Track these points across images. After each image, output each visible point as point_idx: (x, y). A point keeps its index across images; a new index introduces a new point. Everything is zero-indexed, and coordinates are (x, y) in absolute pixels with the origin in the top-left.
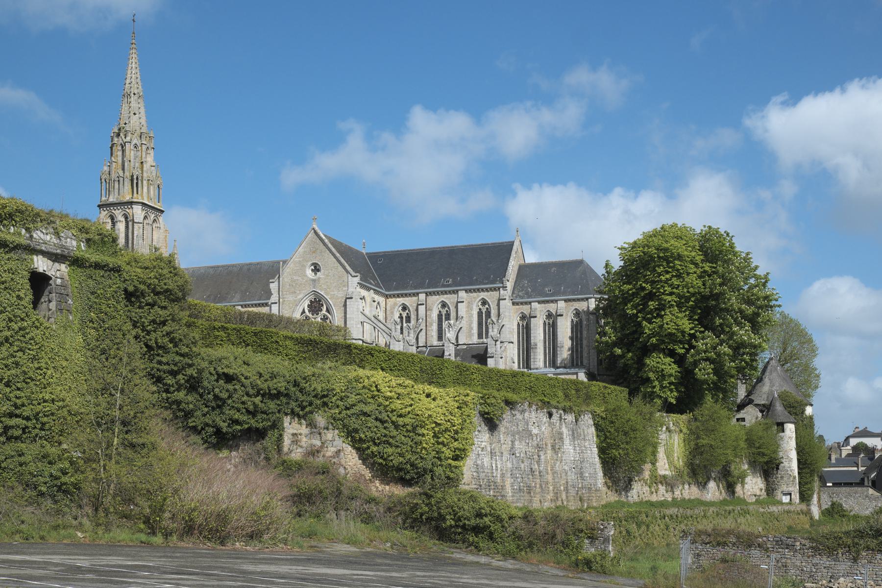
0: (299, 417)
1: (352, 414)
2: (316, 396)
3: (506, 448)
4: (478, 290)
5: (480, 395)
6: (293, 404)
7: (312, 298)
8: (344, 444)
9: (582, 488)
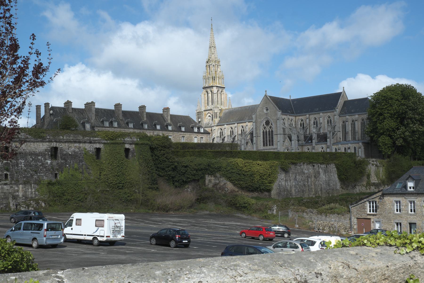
0: (211, 175)
2: (216, 169)
5: (280, 162)
9: (329, 189)
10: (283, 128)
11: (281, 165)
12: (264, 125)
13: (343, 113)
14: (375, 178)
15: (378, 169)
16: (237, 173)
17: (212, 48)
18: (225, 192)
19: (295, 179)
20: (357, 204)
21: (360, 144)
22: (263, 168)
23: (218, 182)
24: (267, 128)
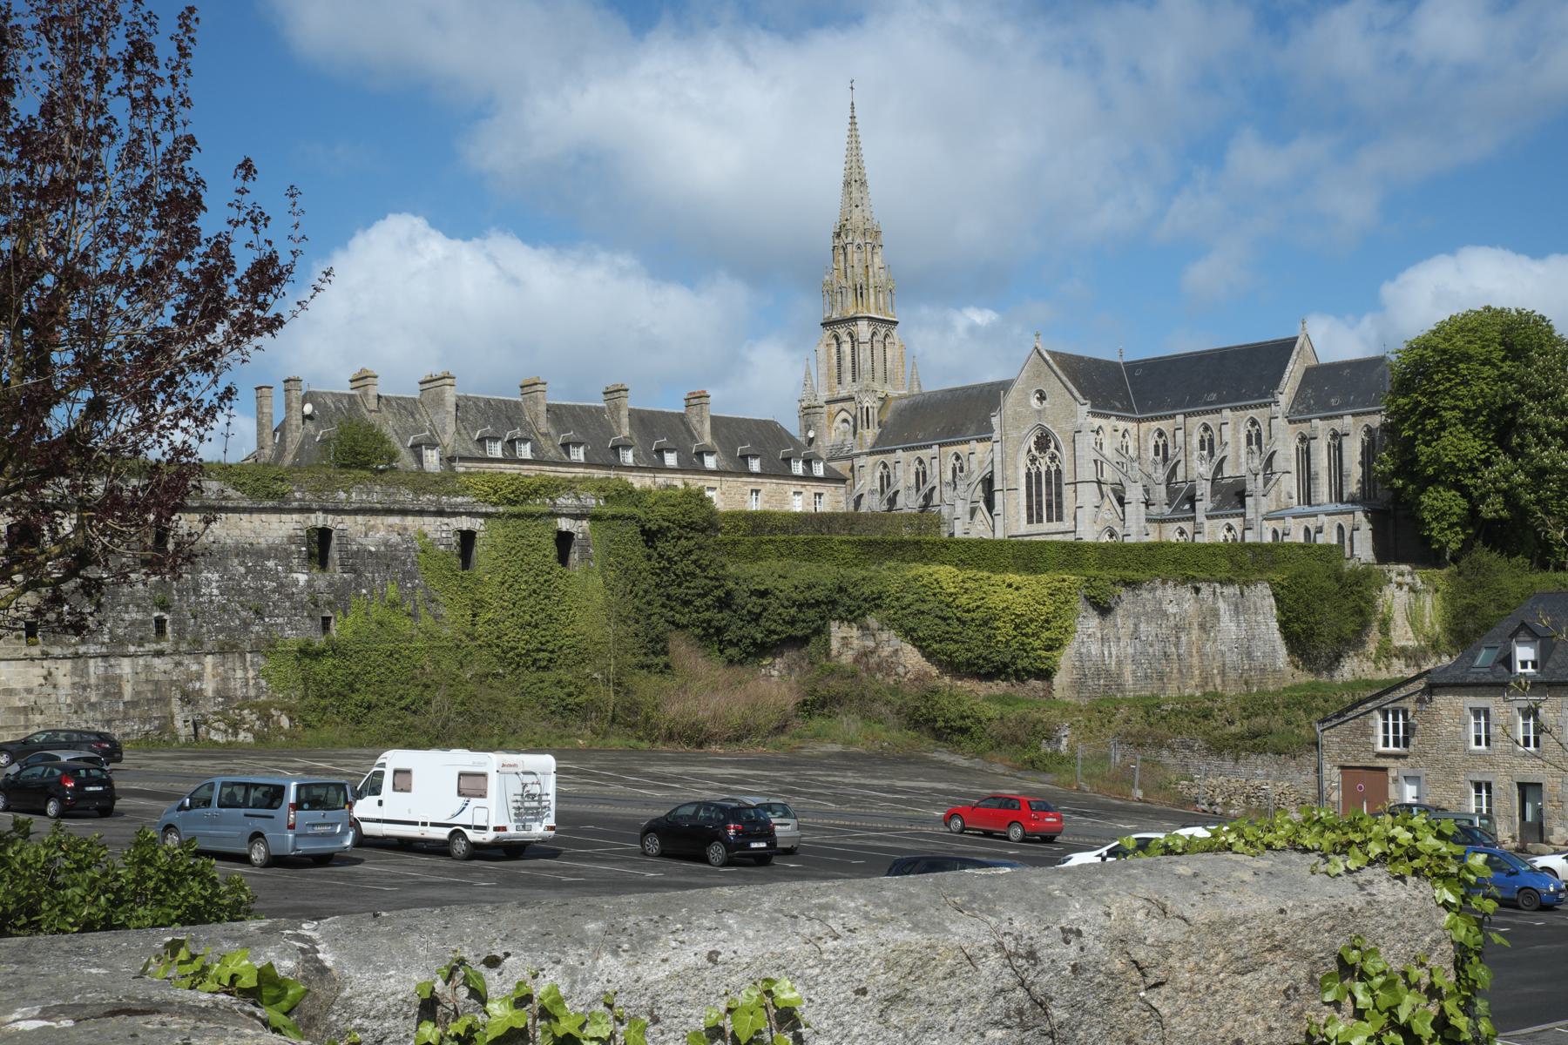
0: (849, 622)
2: (865, 600)
4: (1246, 407)
6: (840, 610)
7: (1038, 433)
10: (1096, 461)
12: (1030, 451)
15: (1417, 599)
19: (1135, 635)
20: (1342, 720)
21: (1360, 515)
23: (871, 644)
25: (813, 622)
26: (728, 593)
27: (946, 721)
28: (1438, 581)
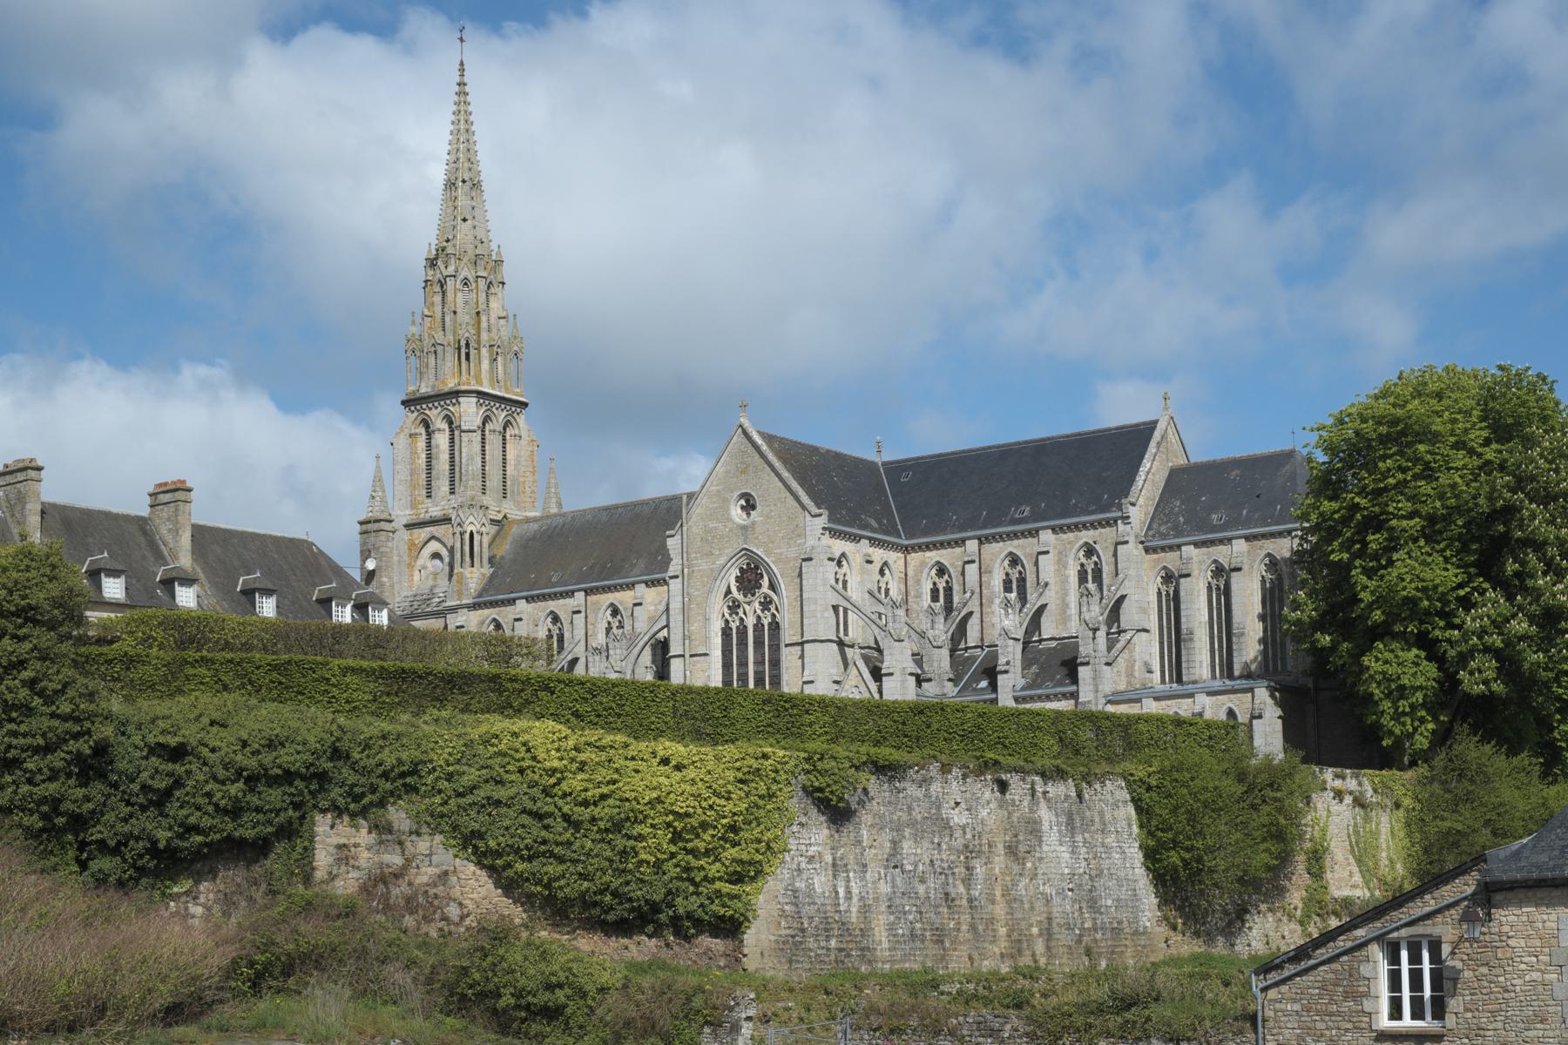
0: (353, 815)
1: (470, 805)
2: (385, 775)
3: (876, 855)
4: (1076, 527)
5: (802, 755)
6: (335, 793)
7: (743, 563)
8: (457, 860)
10: (835, 608)
11: (808, 772)
12: (728, 592)
13: (1163, 529)
14: (1351, 873)
15: (1367, 819)
16: (524, 811)
17: (462, 189)
18: (441, 930)
19: (893, 861)
20: (1303, 965)
21: (1262, 694)
22: (693, 781)
23: (395, 859)
24: (747, 608)
25: (278, 812)
26: (101, 750)
27: (518, 995)
28: (1399, 790)
